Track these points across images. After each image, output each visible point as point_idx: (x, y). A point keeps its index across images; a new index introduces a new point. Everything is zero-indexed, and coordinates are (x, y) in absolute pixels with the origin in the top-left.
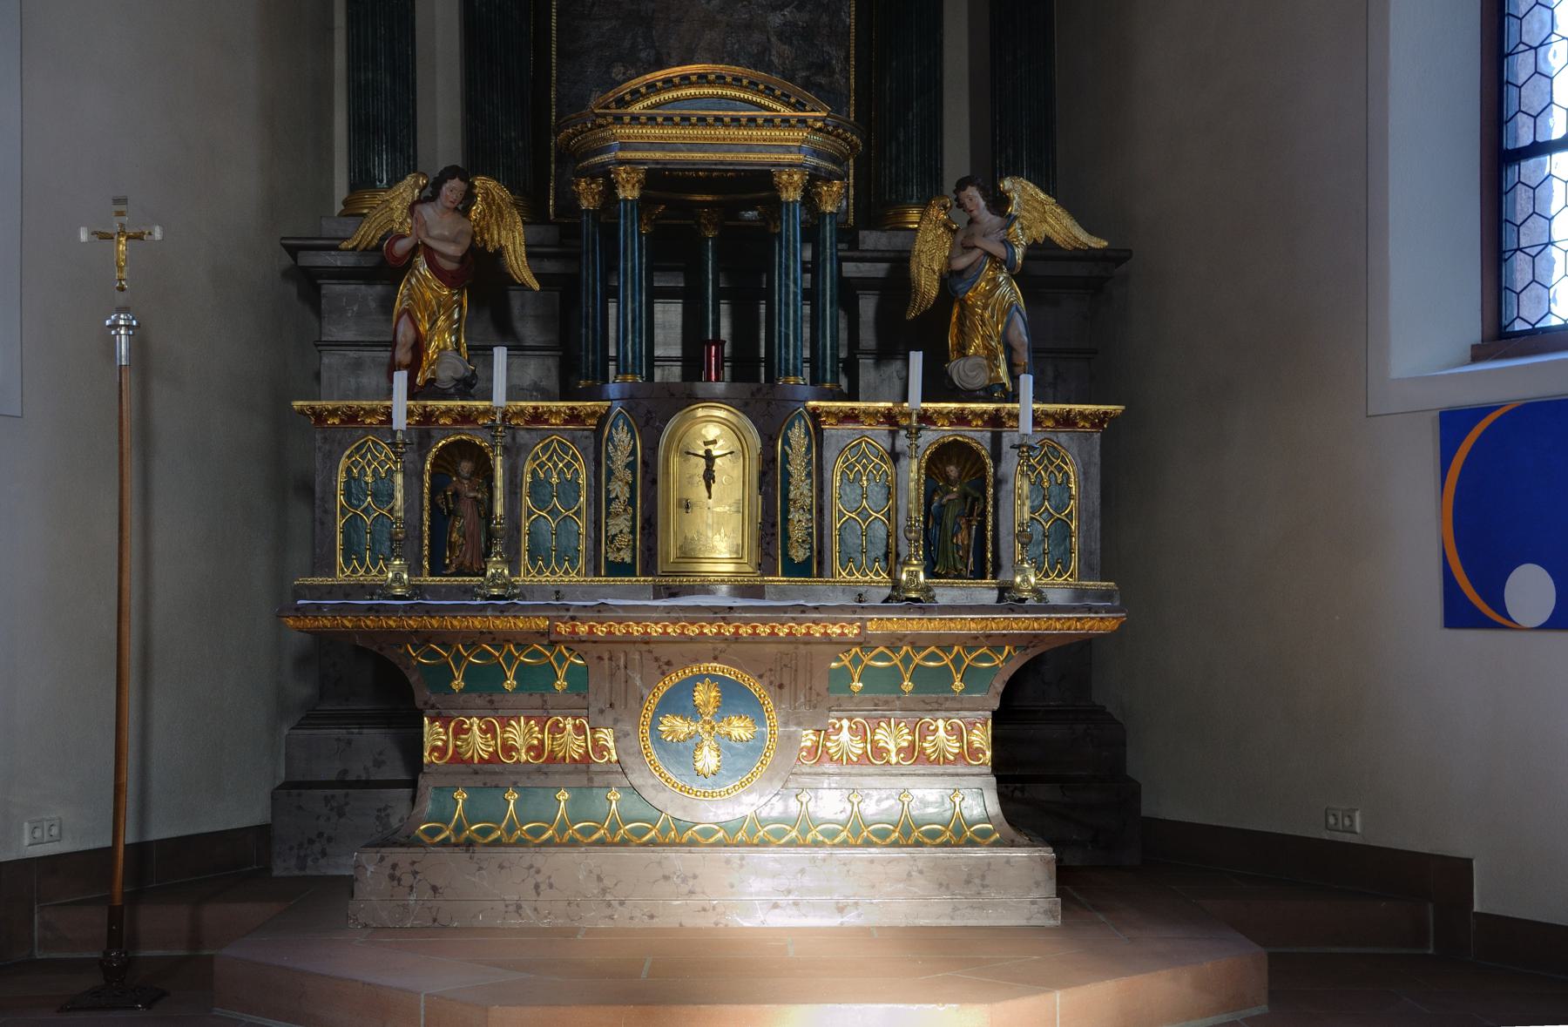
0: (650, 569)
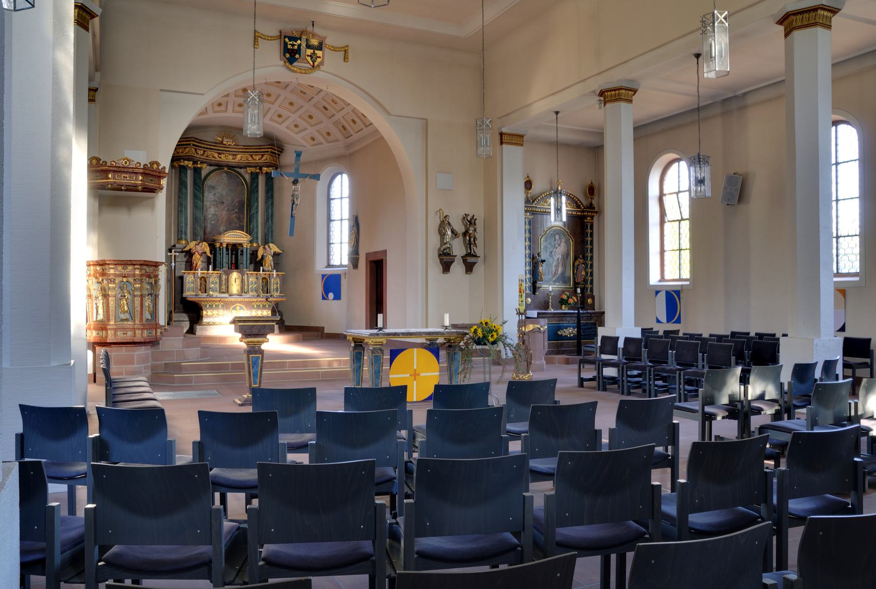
0: (579, 353)
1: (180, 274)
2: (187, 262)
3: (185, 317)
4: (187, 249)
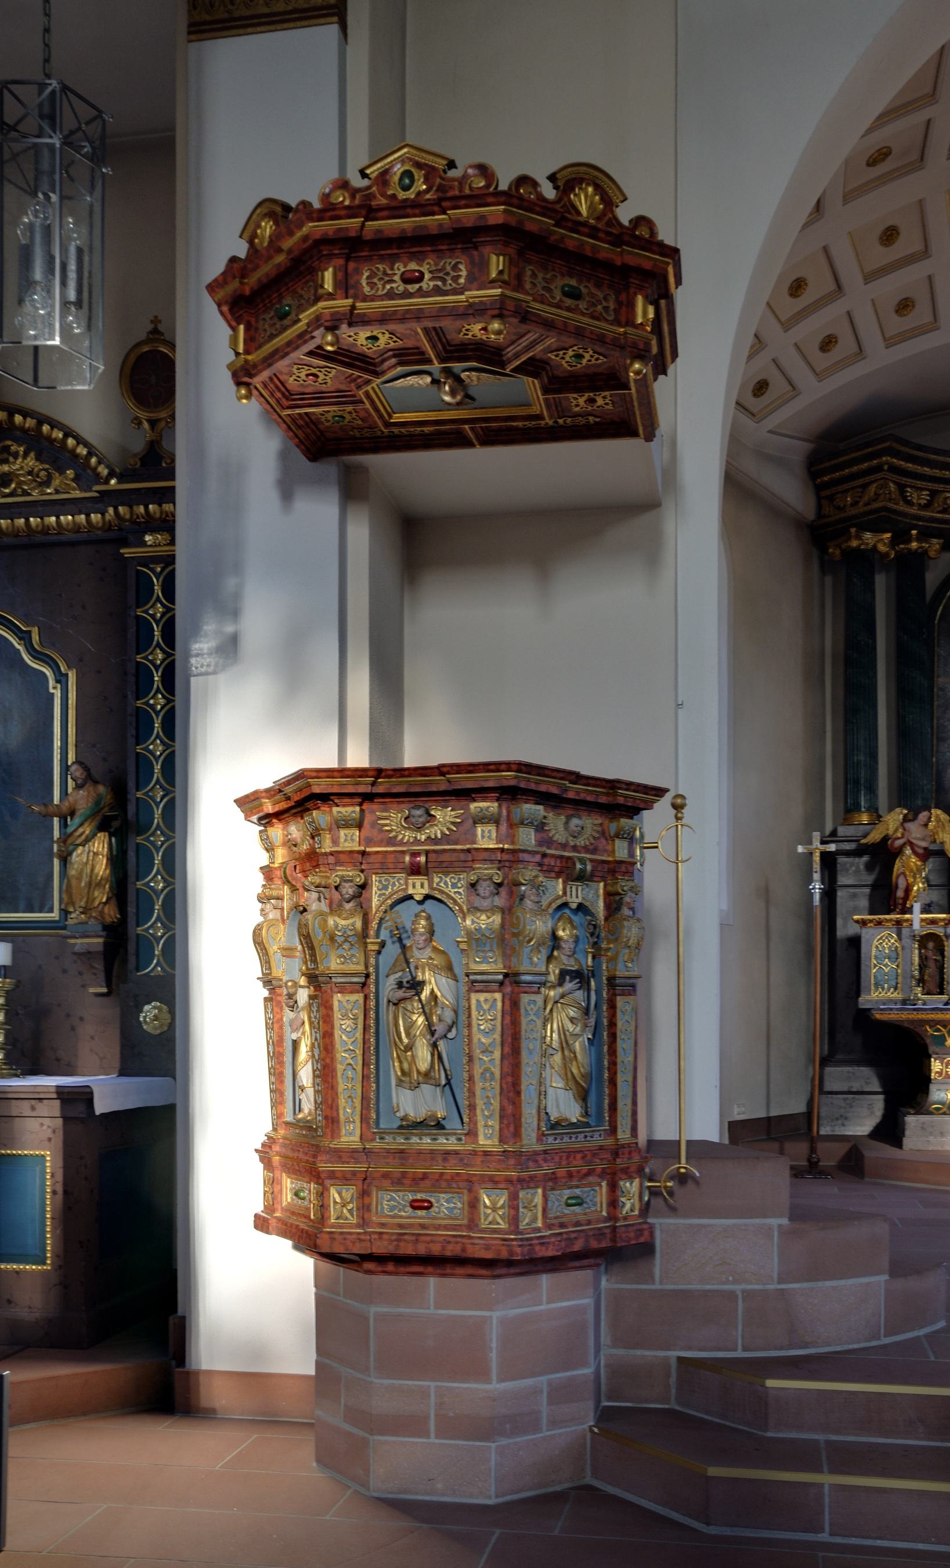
1: (852, 929)
2: (874, 887)
3: (867, 1078)
4: (875, 836)
